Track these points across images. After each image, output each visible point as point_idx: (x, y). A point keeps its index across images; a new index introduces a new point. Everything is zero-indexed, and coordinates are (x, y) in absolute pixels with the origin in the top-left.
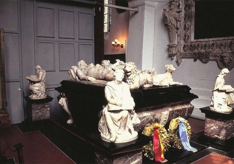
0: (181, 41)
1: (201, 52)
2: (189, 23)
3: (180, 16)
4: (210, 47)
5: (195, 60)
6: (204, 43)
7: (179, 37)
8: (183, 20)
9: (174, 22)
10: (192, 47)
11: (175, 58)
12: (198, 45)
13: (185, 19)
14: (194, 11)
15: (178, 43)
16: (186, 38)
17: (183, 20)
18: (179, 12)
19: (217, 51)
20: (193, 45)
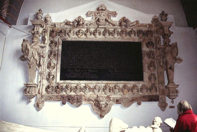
0: (44, 80)
1: (70, 95)
2: (54, 61)
3: (44, 52)
4: (81, 89)
5: (64, 103)
6: (75, 85)
7: (41, 75)
8: (47, 57)
9: (37, 57)
10: (58, 88)
11: (33, 101)
12: (66, 87)
13: (49, 56)
14: (61, 50)
15: (40, 82)
16: (49, 77)
17: (47, 56)
18: (42, 47)
19: (89, 94)
20: (60, 87)
